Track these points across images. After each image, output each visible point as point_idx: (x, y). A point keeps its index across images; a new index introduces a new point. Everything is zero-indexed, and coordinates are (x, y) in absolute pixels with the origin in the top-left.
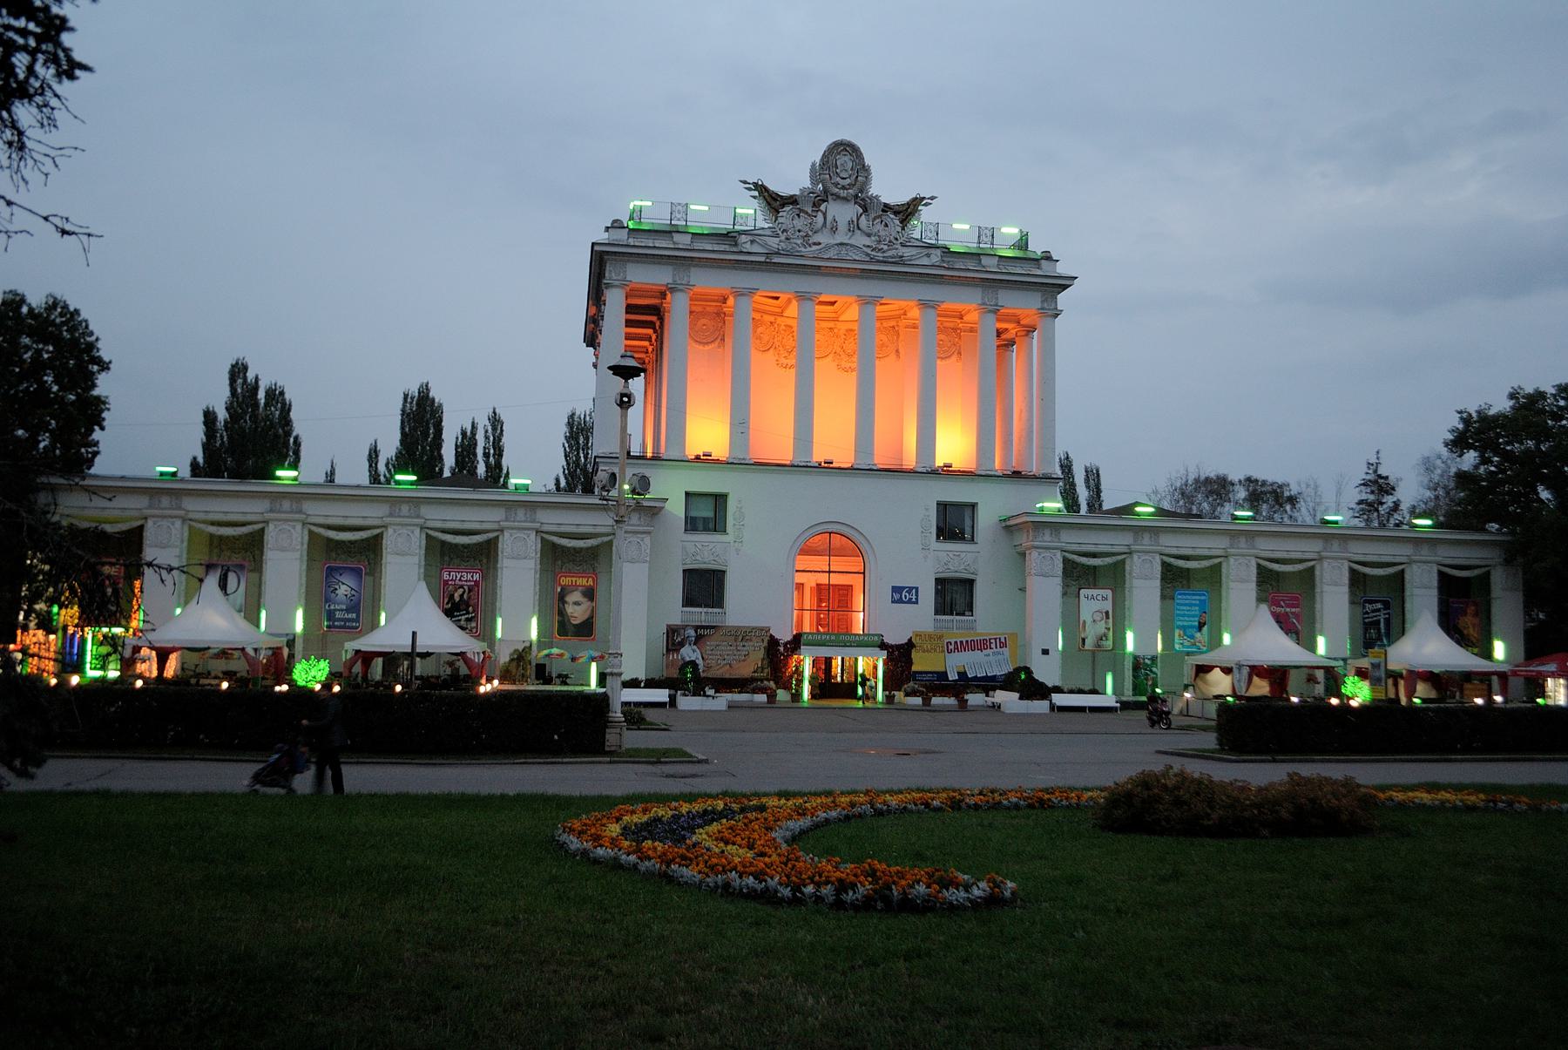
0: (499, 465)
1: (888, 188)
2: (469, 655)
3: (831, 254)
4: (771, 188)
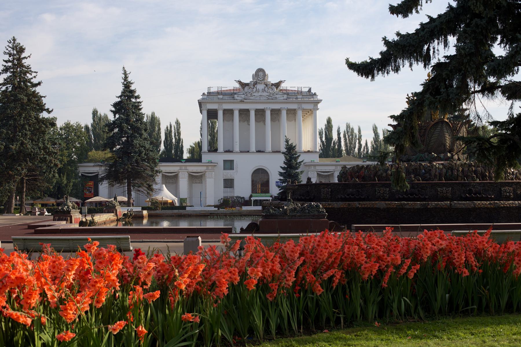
0: (179, 139)
1: (272, 79)
2: (6, 298)
3: (258, 98)
4: (242, 81)
